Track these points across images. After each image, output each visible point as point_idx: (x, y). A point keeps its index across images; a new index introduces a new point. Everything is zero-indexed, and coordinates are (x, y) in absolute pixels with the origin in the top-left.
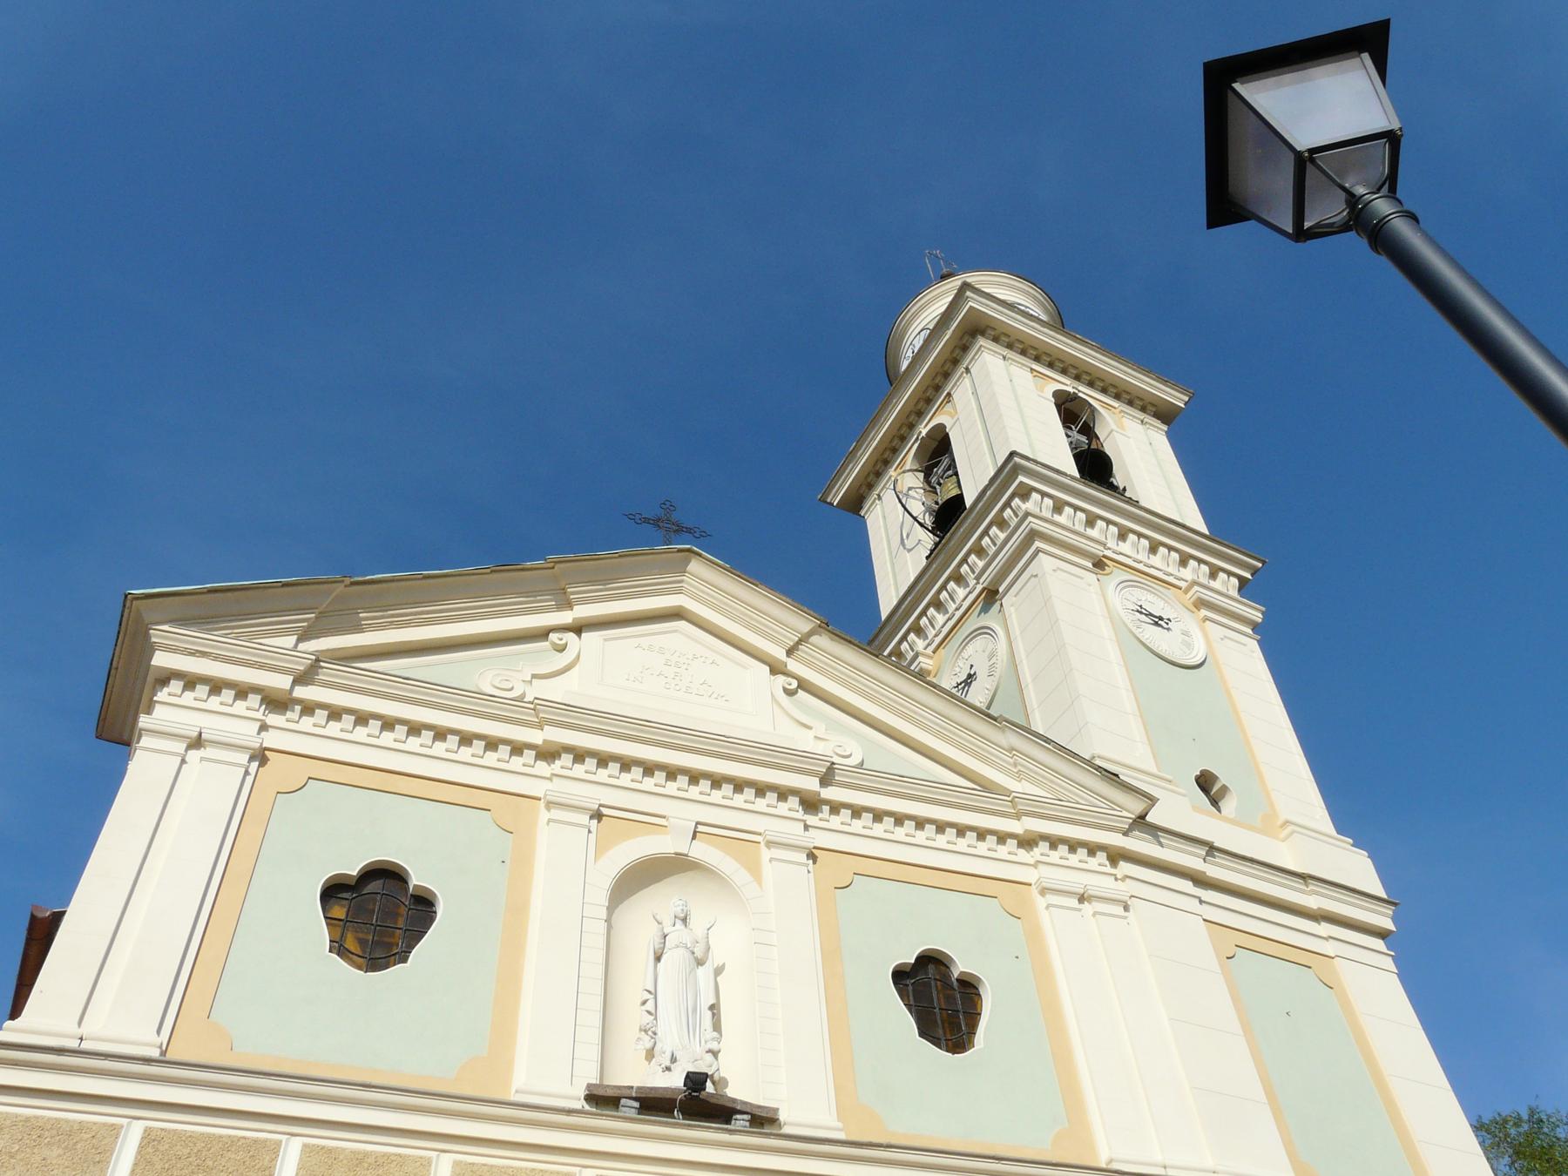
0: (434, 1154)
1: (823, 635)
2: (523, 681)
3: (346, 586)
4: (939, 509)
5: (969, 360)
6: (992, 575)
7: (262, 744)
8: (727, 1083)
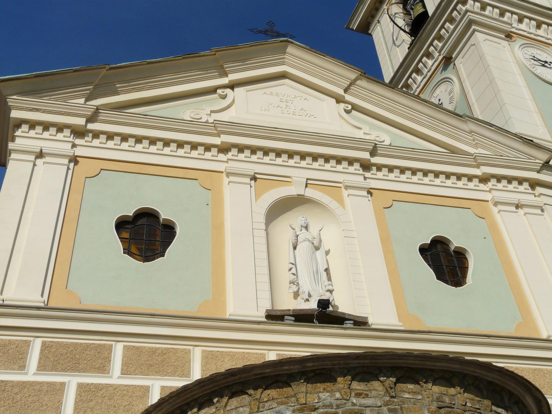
0: (191, 347)
1: (363, 80)
2: (207, 114)
3: (107, 70)
4: (413, 22)
5: (373, 26)
6: (461, 29)
7: (74, 153)
8: (338, 307)
